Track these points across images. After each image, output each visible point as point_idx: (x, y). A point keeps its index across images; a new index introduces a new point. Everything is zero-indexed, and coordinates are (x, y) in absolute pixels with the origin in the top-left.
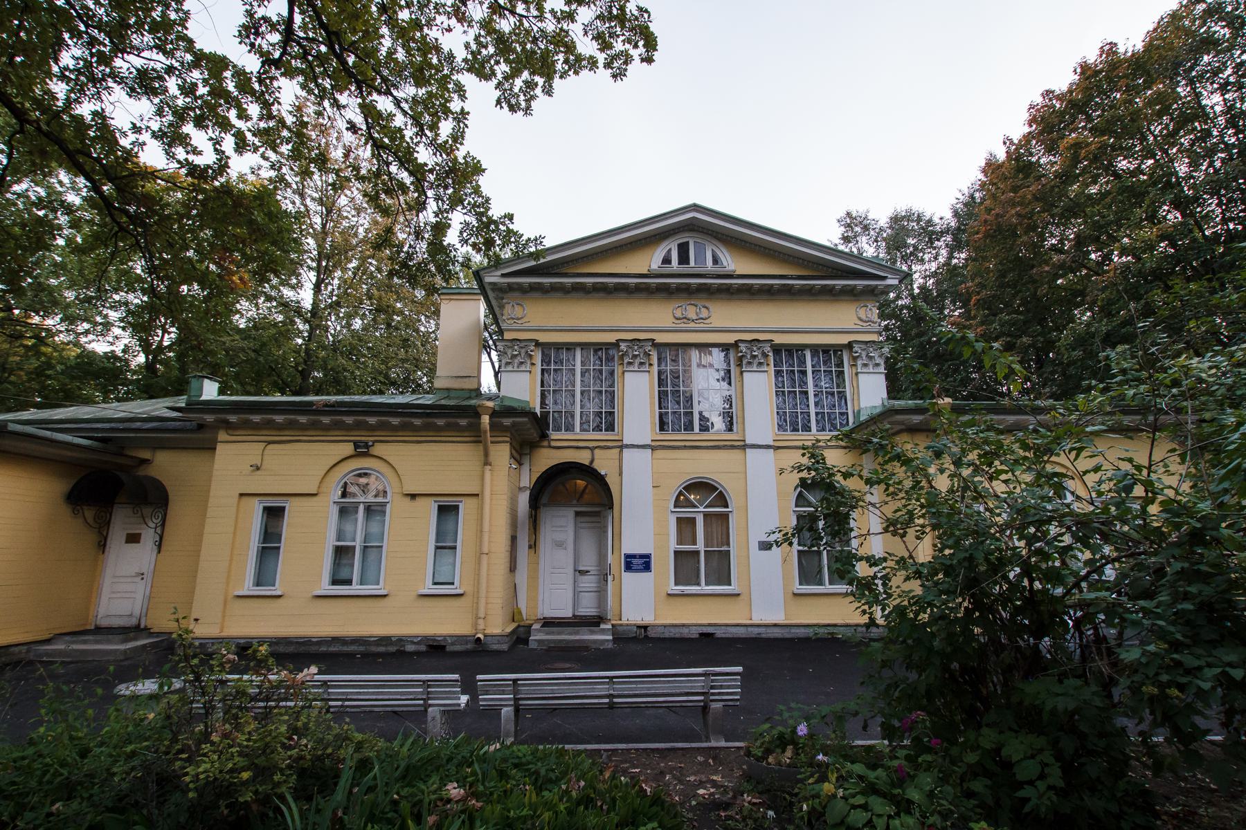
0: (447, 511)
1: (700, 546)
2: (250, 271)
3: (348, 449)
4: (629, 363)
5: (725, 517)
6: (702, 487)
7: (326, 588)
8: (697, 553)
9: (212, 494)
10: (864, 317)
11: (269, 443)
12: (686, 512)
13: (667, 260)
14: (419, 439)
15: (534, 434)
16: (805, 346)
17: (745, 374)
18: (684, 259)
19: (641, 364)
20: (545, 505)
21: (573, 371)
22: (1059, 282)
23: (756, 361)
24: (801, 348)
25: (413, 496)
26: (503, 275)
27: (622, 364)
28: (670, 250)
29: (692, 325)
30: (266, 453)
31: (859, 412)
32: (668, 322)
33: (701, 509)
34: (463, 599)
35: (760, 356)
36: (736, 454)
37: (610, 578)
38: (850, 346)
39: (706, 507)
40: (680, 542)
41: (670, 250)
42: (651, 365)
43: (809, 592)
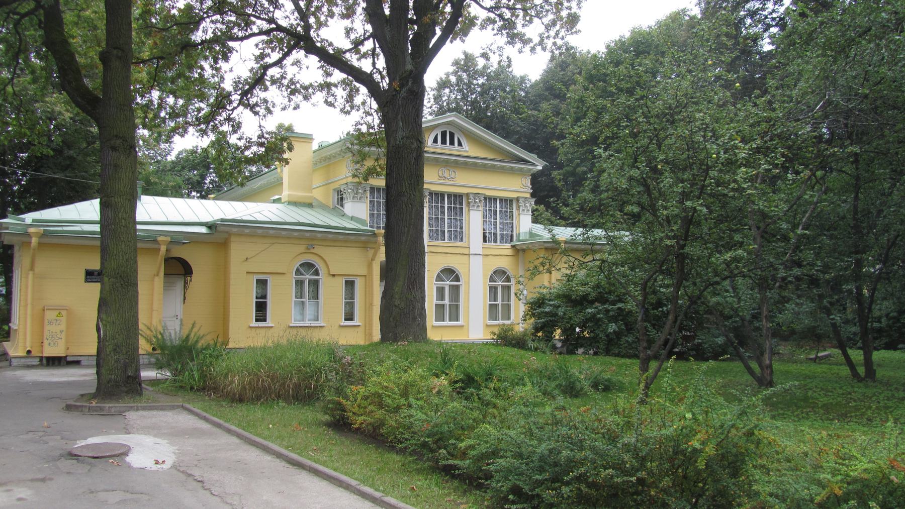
0: (350, 285)
1: (499, 302)
3: (302, 248)
5: (457, 287)
6: (308, 266)
14: (324, 244)
17: (471, 211)
23: (476, 205)
24: (495, 199)
25: (334, 275)
28: (437, 135)
29: (447, 182)
31: (519, 234)
33: (448, 283)
36: (466, 257)
38: (518, 199)
39: (451, 281)
41: (437, 135)
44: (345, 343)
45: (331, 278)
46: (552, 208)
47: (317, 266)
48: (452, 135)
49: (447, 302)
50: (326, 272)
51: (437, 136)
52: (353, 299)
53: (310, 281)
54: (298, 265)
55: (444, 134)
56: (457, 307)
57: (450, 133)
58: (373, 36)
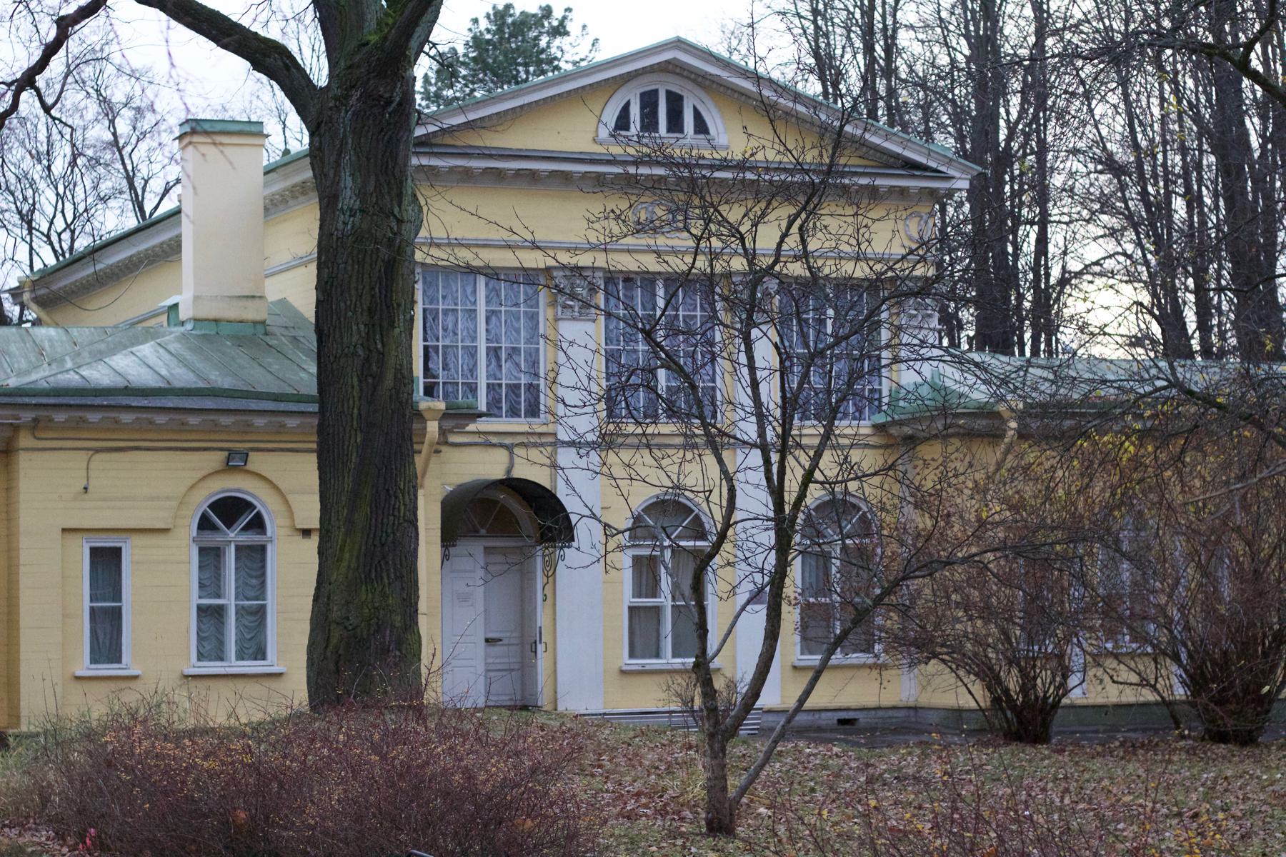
2: (1116, 642)
3: (216, 459)
7: (84, 666)
11: (97, 451)
21: (472, 313)
28: (627, 105)
30: (91, 466)
37: (540, 648)
40: (638, 593)
41: (627, 105)
44: (257, 716)
45: (299, 538)
46: (678, 165)
47: (259, 507)
48: (675, 102)
49: (230, 600)
50: (287, 522)
51: (626, 109)
52: (120, 600)
53: (238, 548)
54: (205, 506)
55: (649, 101)
56: (261, 612)
57: (669, 93)
58: (968, 191)
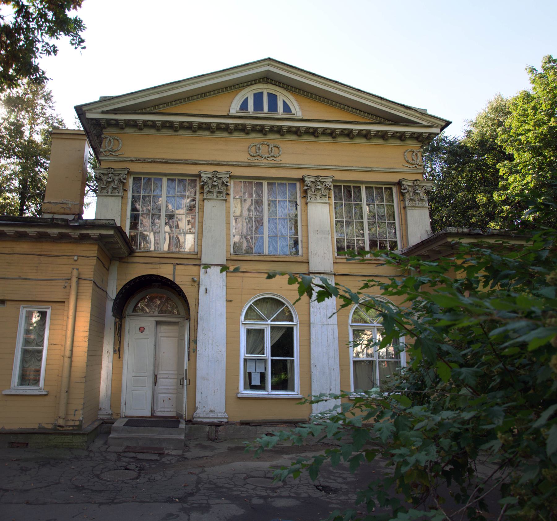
4: (209, 192)
8: (265, 361)
9: (89, 318)
10: (410, 160)
12: (256, 324)
13: (244, 106)
15: (124, 250)
16: (362, 182)
18: (258, 105)
19: (219, 192)
20: (129, 315)
22: (444, 220)
26: (103, 112)
27: (203, 193)
32: (244, 158)
33: (269, 322)
34: (47, 398)
35: (323, 190)
41: (247, 99)
42: (228, 194)
43: (24, 393)
